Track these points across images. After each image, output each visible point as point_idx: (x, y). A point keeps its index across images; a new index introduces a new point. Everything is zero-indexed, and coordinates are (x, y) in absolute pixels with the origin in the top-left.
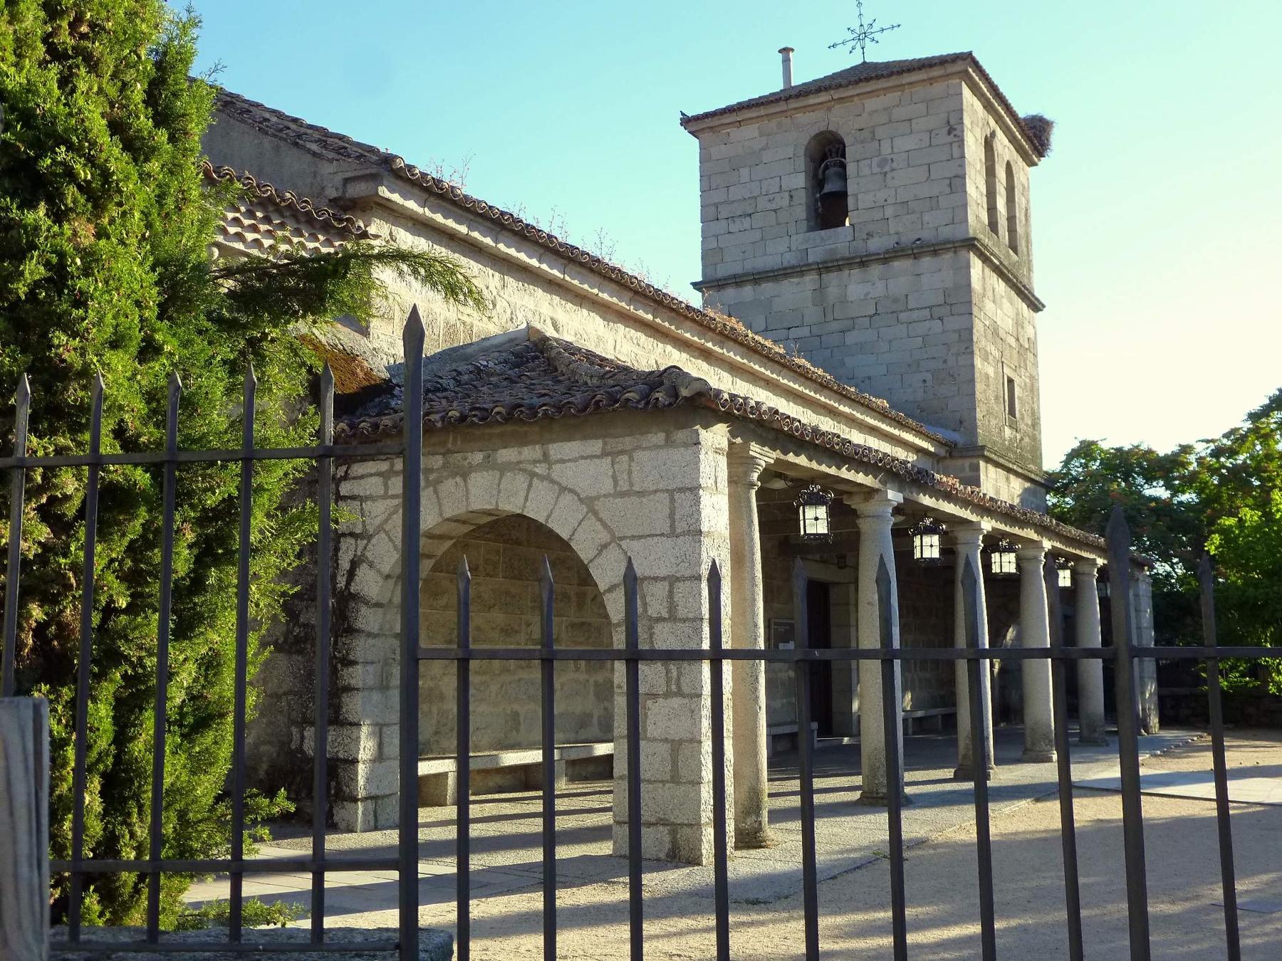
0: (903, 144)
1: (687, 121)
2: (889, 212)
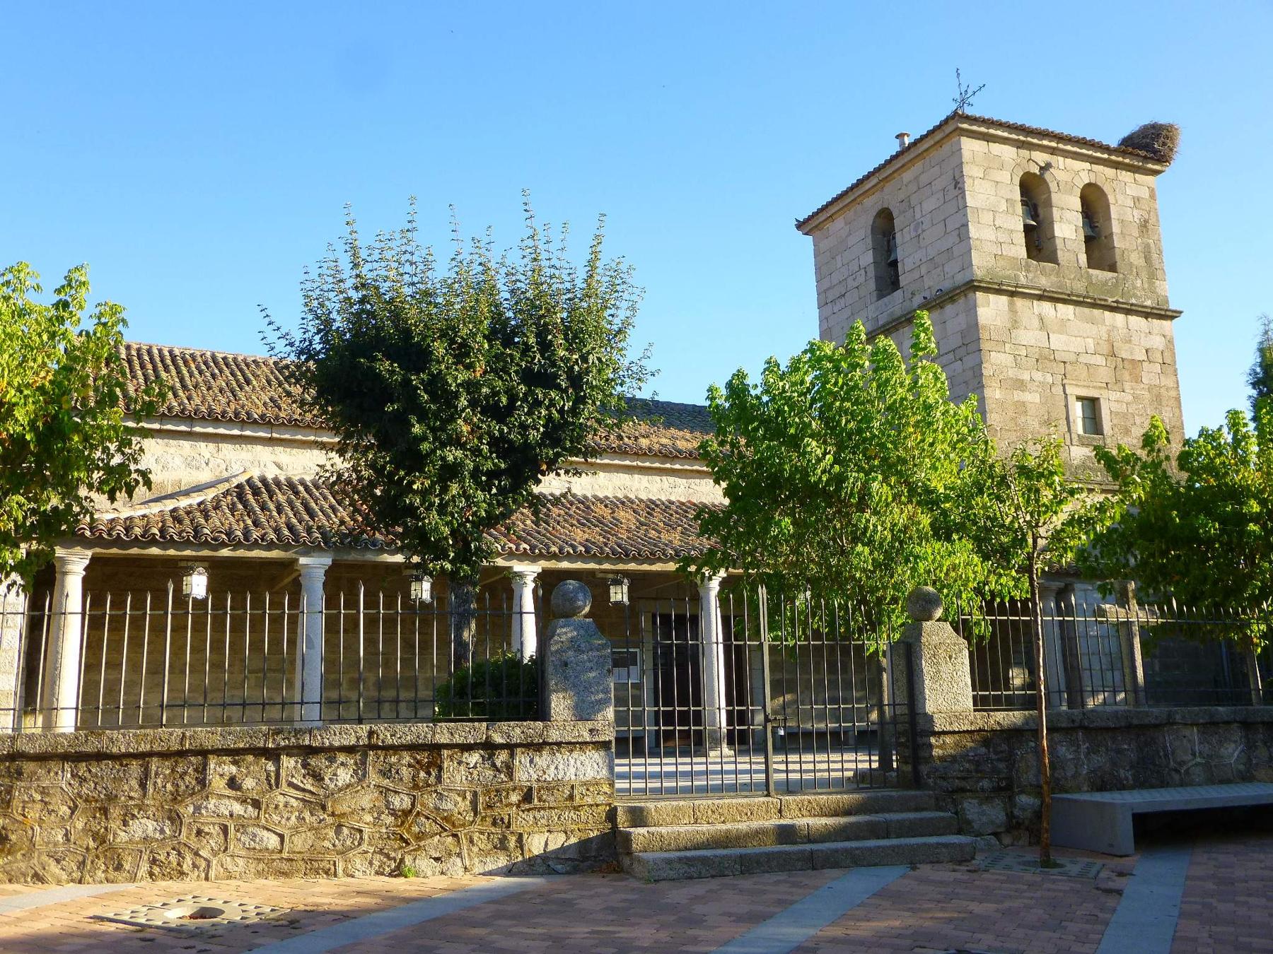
0: (929, 205)
1: (800, 225)
2: (924, 270)
